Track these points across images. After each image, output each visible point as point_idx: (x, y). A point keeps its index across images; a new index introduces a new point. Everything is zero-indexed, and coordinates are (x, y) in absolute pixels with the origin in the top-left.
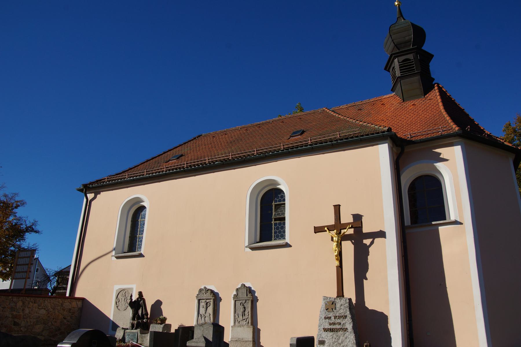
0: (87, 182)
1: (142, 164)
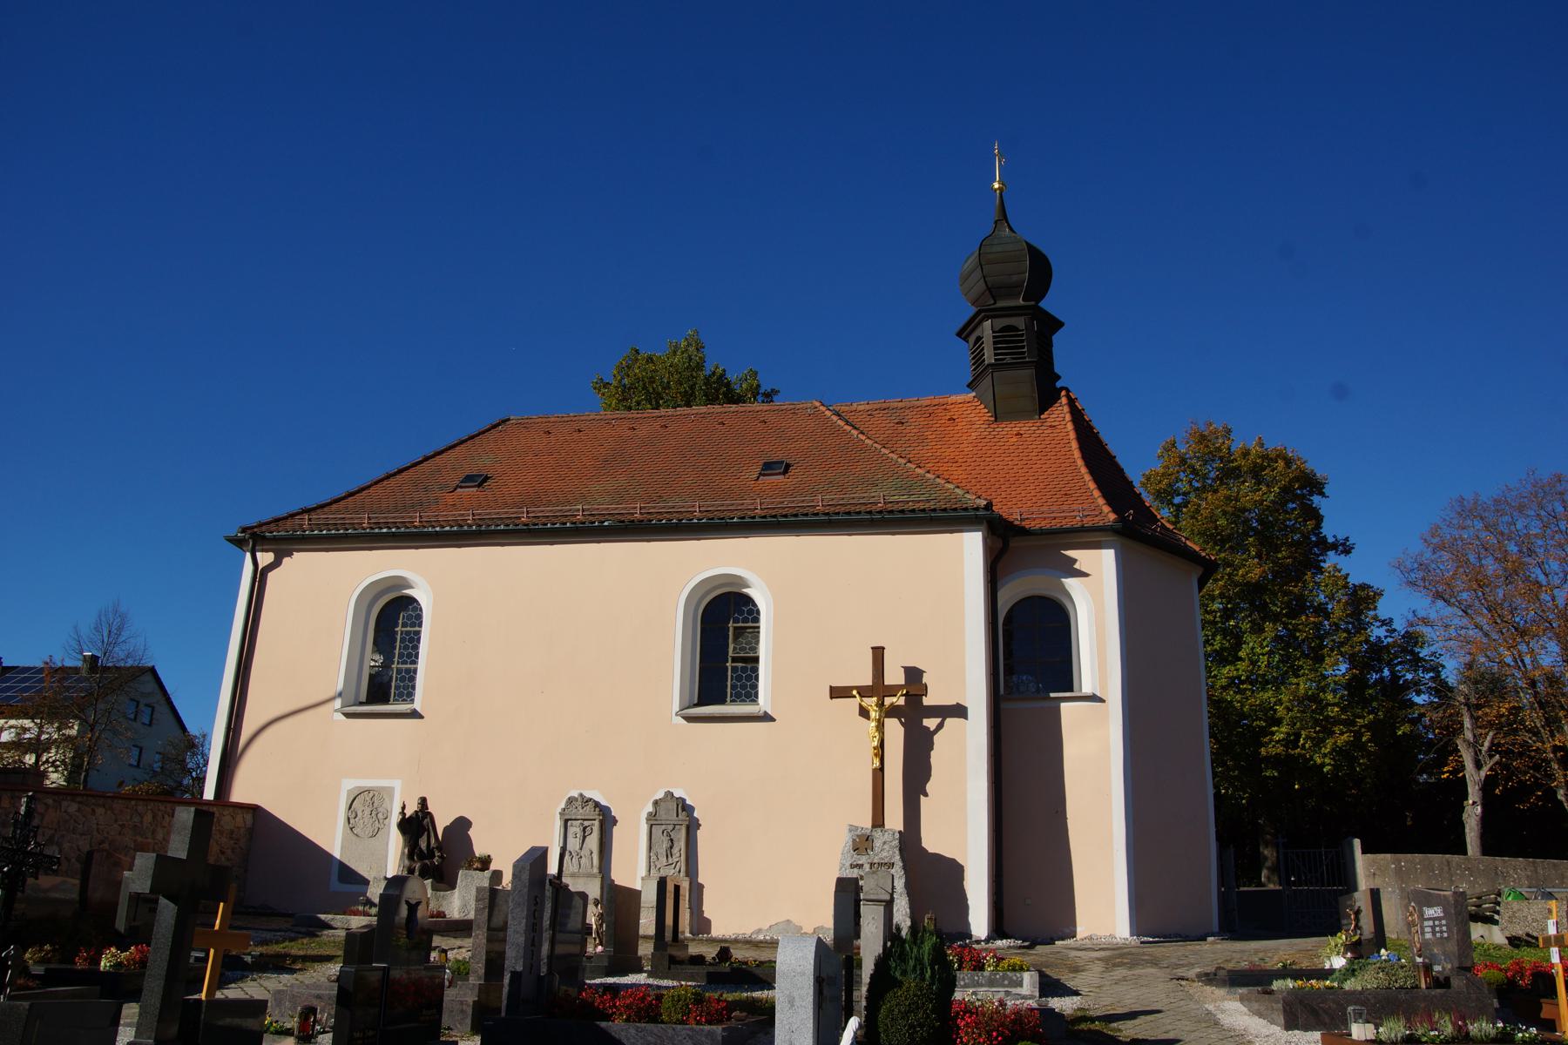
0: (252, 521)
1: (376, 483)
